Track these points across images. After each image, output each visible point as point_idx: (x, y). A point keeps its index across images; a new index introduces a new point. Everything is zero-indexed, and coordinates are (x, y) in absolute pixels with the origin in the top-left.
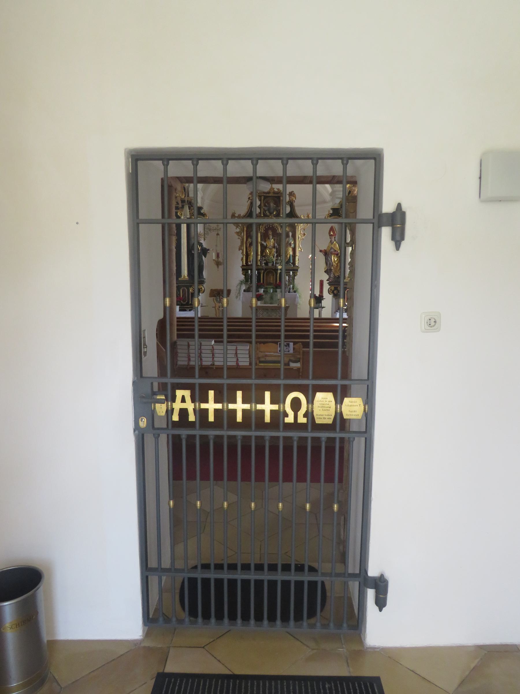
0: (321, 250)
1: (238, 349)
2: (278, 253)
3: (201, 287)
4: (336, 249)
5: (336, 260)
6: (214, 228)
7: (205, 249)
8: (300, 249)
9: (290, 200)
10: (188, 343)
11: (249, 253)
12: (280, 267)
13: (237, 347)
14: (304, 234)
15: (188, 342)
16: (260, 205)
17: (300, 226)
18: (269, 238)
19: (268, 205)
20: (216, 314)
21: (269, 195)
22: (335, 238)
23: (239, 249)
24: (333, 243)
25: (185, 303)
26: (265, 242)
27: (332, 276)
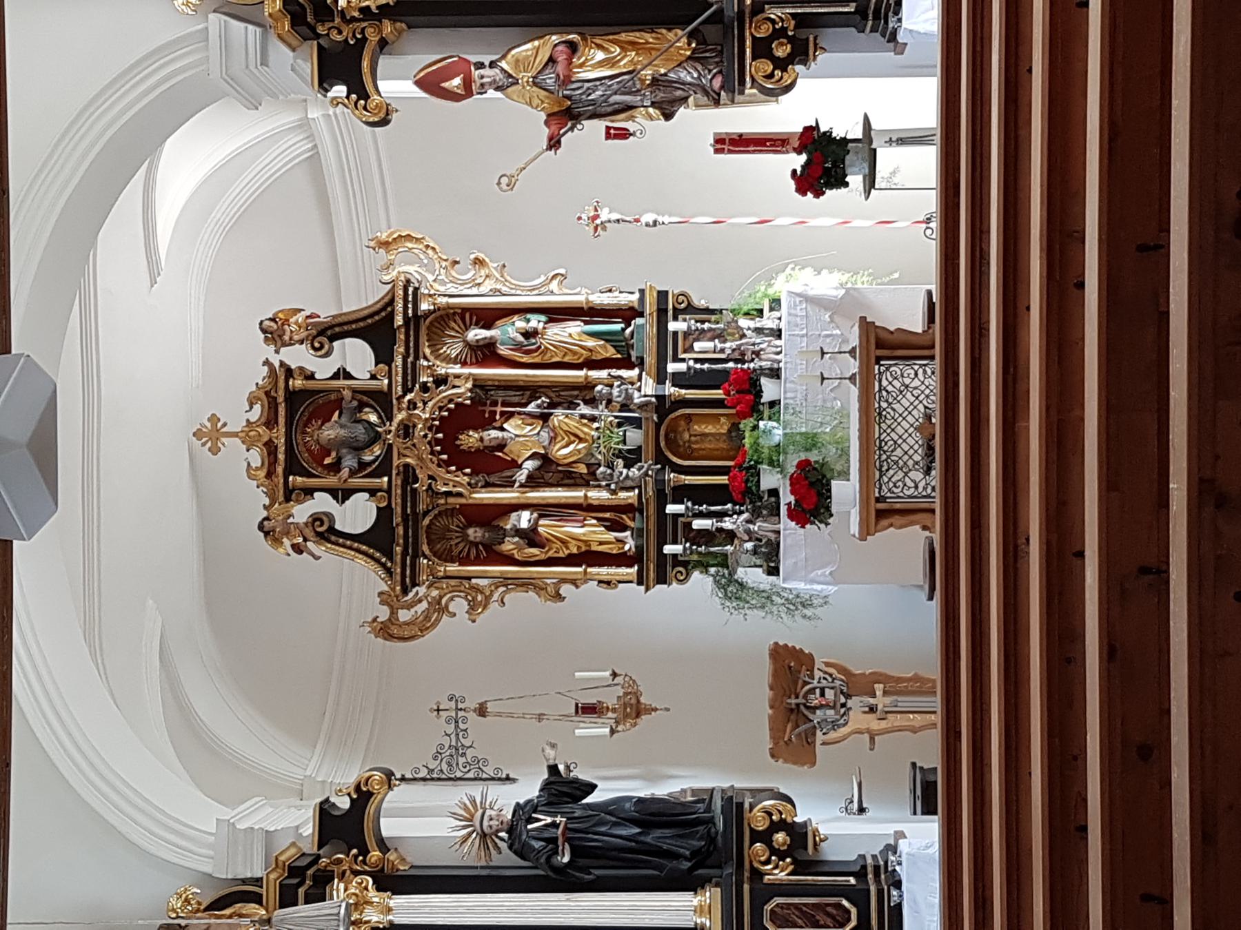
0: (550, 139)
2: (576, 397)
3: (757, 812)
4: (544, 56)
5: (600, 56)
6: (451, 728)
7: (546, 786)
8: (554, 286)
9: (307, 337)
11: (575, 551)
12: (649, 387)
14: (478, 262)
16: (333, 492)
17: (436, 286)
18: (501, 446)
19: (334, 454)
21: (282, 449)
22: (480, 66)
23: (558, 597)
24: (510, 76)
26: (520, 467)
27: (687, 75)
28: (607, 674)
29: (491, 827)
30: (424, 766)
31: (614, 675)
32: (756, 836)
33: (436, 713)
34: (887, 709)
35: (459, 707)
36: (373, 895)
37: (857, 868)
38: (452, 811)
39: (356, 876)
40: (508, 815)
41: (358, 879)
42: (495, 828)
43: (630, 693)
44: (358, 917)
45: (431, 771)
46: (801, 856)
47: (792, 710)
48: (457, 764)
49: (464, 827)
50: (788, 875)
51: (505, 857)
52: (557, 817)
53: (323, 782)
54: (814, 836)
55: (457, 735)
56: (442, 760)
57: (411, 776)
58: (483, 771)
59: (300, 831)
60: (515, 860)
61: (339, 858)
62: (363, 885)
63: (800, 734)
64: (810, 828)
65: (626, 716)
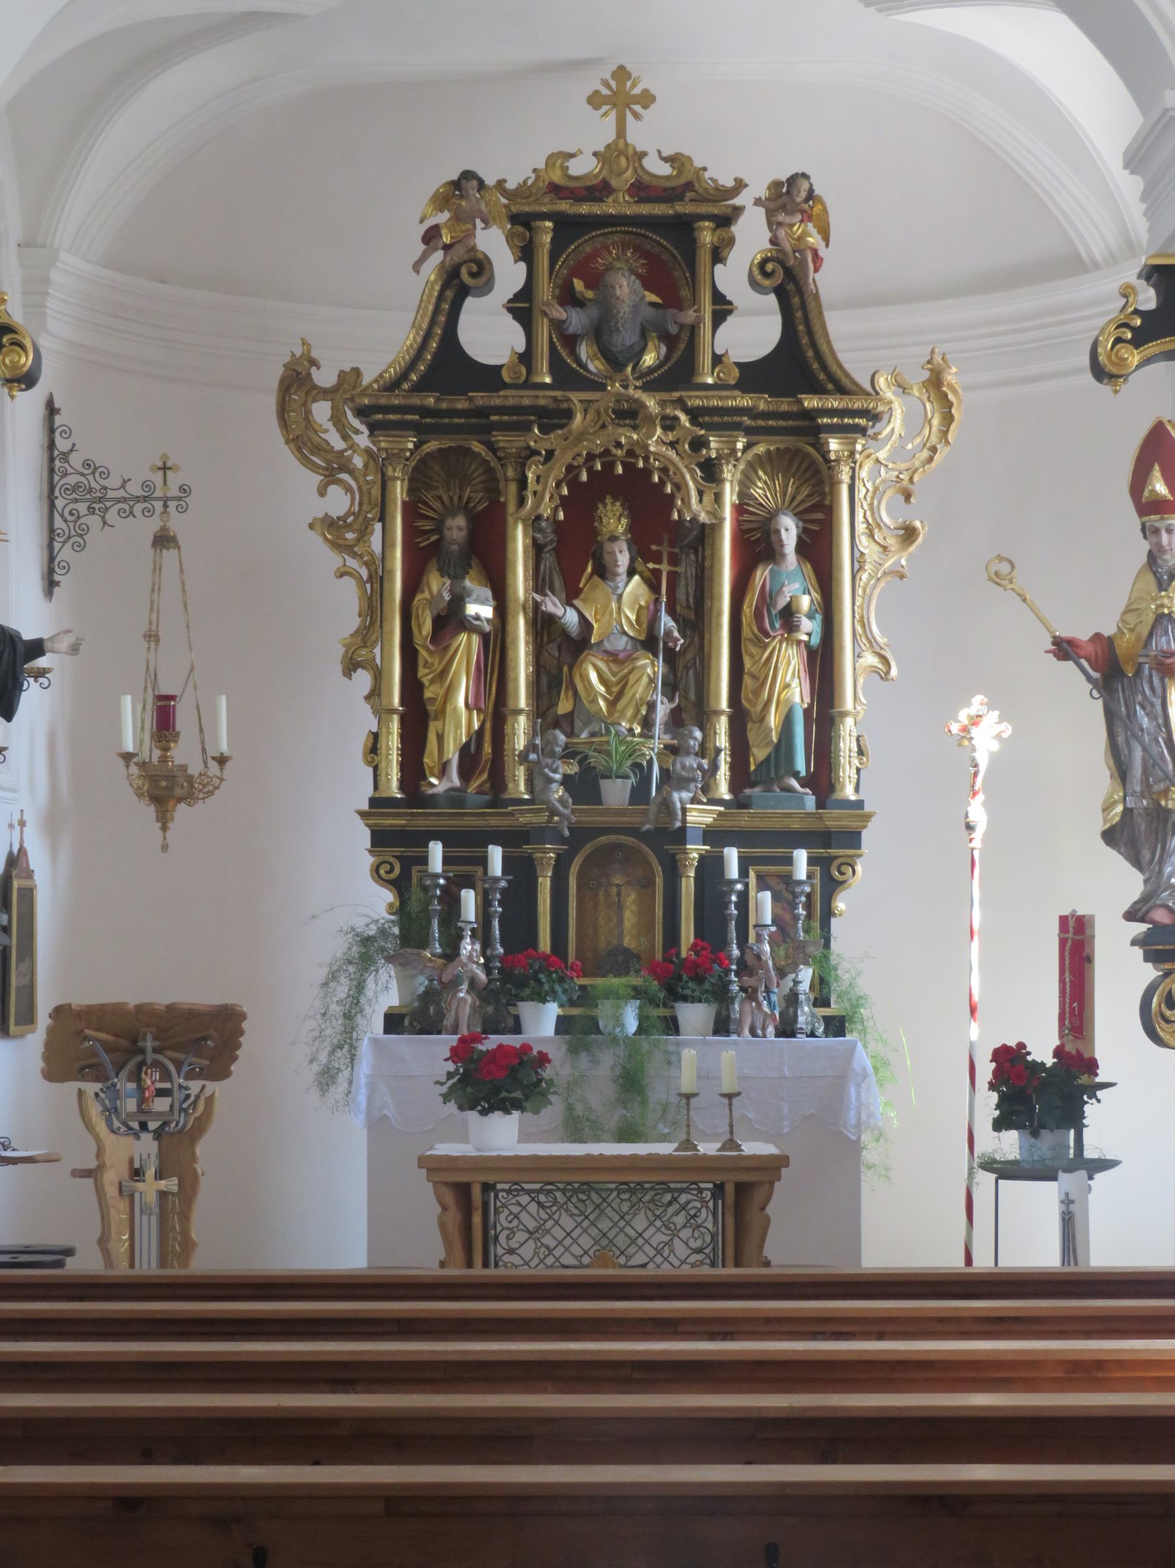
0: (1071, 642)
6: (135, 489)
28: (224, 747)
30: (74, 445)
31: (222, 760)
33: (160, 464)
34: (137, 1196)
35: (169, 503)
43: (191, 786)
45: (65, 456)
47: (134, 1041)
48: (76, 501)
55: (125, 500)
56: (83, 475)
58: (64, 543)
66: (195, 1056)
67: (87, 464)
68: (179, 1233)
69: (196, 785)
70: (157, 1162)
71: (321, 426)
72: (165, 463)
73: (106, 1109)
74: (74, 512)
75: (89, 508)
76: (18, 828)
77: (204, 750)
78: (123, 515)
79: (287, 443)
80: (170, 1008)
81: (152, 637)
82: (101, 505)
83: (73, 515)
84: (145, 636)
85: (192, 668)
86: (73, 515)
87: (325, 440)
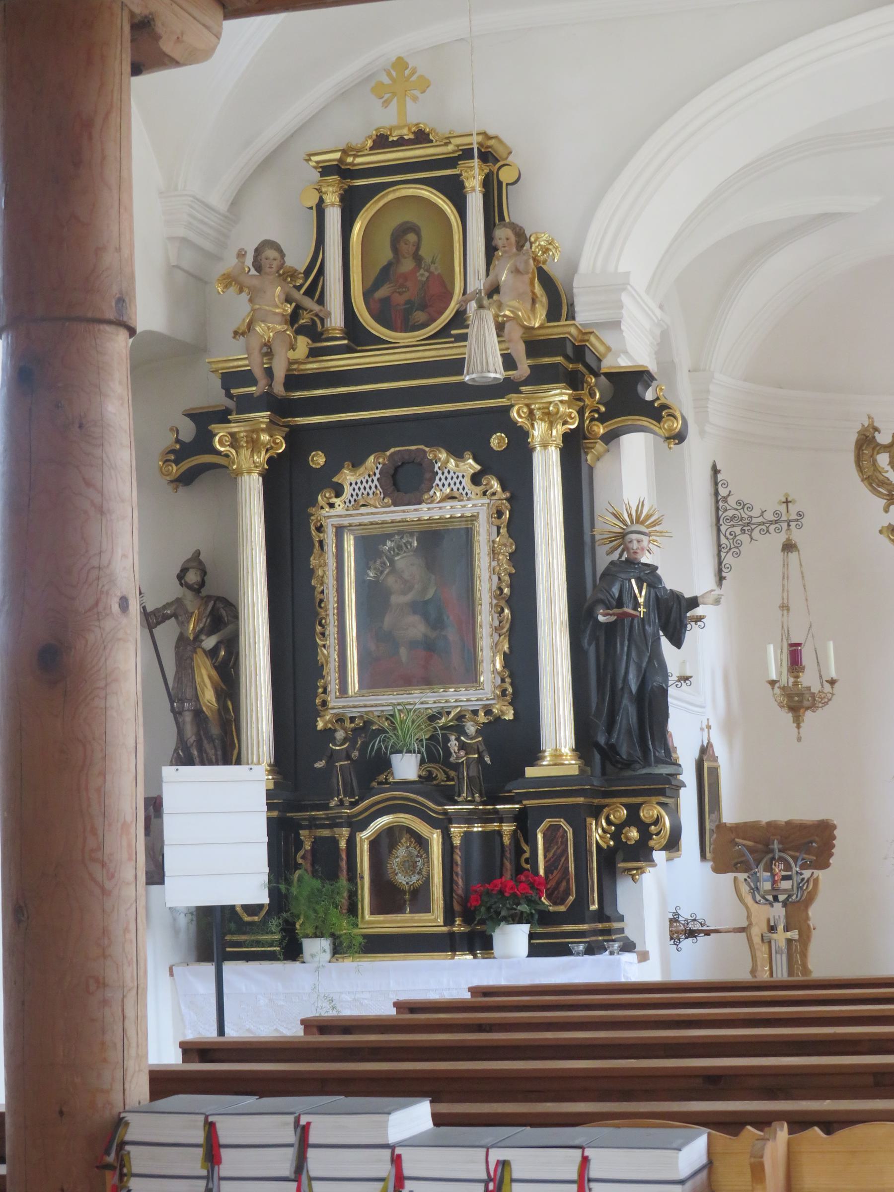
1: (594, 1172)
6: (769, 516)
7: (676, 597)
10: (211, 1128)
13: (585, 1160)
15: (207, 1117)
20: (753, 972)
25: (562, 908)
28: (833, 674)
29: (631, 542)
30: (730, 492)
31: (832, 682)
32: (633, 810)
33: (784, 500)
34: (773, 943)
35: (791, 523)
36: (559, 430)
37: (608, 911)
38: (644, 503)
39: (578, 412)
40: (645, 559)
41: (575, 414)
42: (630, 546)
43: (815, 700)
44: (537, 417)
45: (725, 499)
46: (619, 856)
47: (767, 845)
48: (733, 526)
49: (630, 515)
50: (597, 842)
51: (604, 558)
52: (645, 607)
53: (708, 391)
54: (637, 869)
55: (763, 523)
56: (737, 510)
57: (719, 480)
58: (727, 552)
59: (622, 355)
60: (601, 566)
61: (595, 395)
62: (569, 420)
63: (744, 855)
64: (643, 864)
65: (790, 696)
66: (806, 853)
67: (738, 503)
68: (800, 965)
69: (817, 699)
70: (785, 921)
71: (883, 468)
72: (787, 499)
73: (751, 888)
74: (732, 533)
75: (742, 530)
76: (706, 730)
77: (821, 676)
78: (763, 533)
79: (863, 480)
80: (788, 823)
81: (785, 607)
82: (749, 528)
83: (732, 535)
84: (780, 607)
85: (811, 626)
86: (732, 535)
87: (886, 477)
